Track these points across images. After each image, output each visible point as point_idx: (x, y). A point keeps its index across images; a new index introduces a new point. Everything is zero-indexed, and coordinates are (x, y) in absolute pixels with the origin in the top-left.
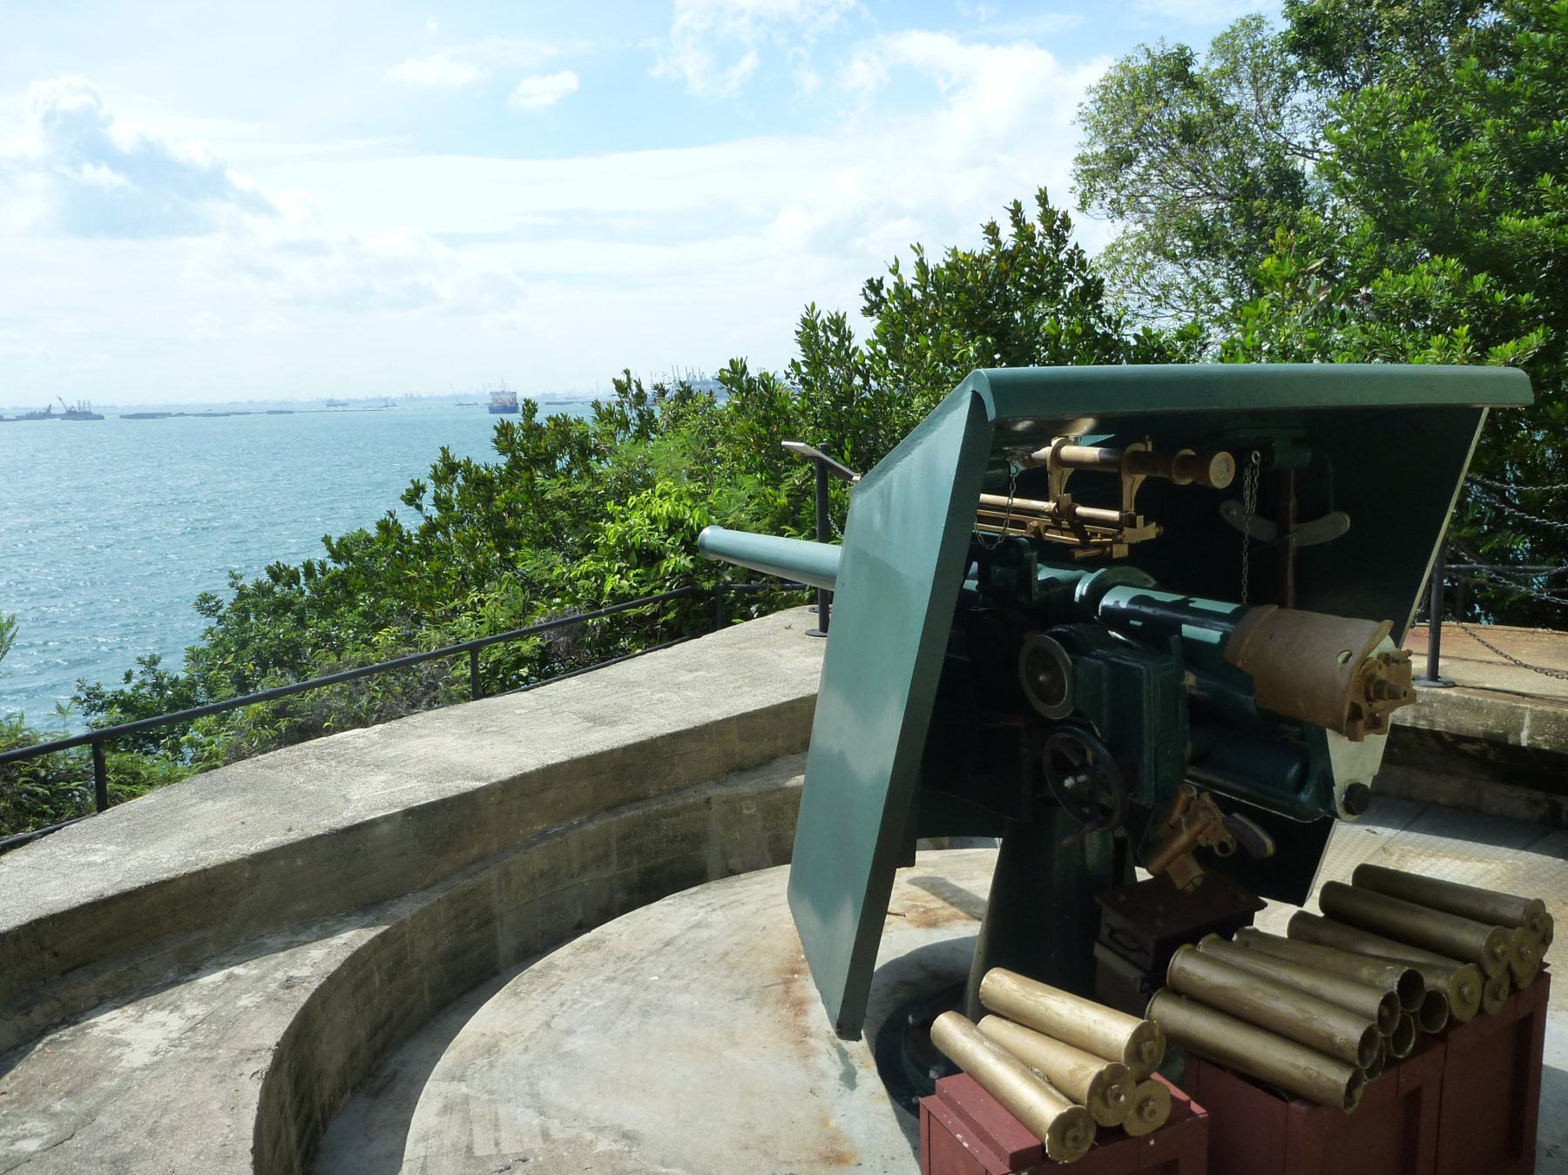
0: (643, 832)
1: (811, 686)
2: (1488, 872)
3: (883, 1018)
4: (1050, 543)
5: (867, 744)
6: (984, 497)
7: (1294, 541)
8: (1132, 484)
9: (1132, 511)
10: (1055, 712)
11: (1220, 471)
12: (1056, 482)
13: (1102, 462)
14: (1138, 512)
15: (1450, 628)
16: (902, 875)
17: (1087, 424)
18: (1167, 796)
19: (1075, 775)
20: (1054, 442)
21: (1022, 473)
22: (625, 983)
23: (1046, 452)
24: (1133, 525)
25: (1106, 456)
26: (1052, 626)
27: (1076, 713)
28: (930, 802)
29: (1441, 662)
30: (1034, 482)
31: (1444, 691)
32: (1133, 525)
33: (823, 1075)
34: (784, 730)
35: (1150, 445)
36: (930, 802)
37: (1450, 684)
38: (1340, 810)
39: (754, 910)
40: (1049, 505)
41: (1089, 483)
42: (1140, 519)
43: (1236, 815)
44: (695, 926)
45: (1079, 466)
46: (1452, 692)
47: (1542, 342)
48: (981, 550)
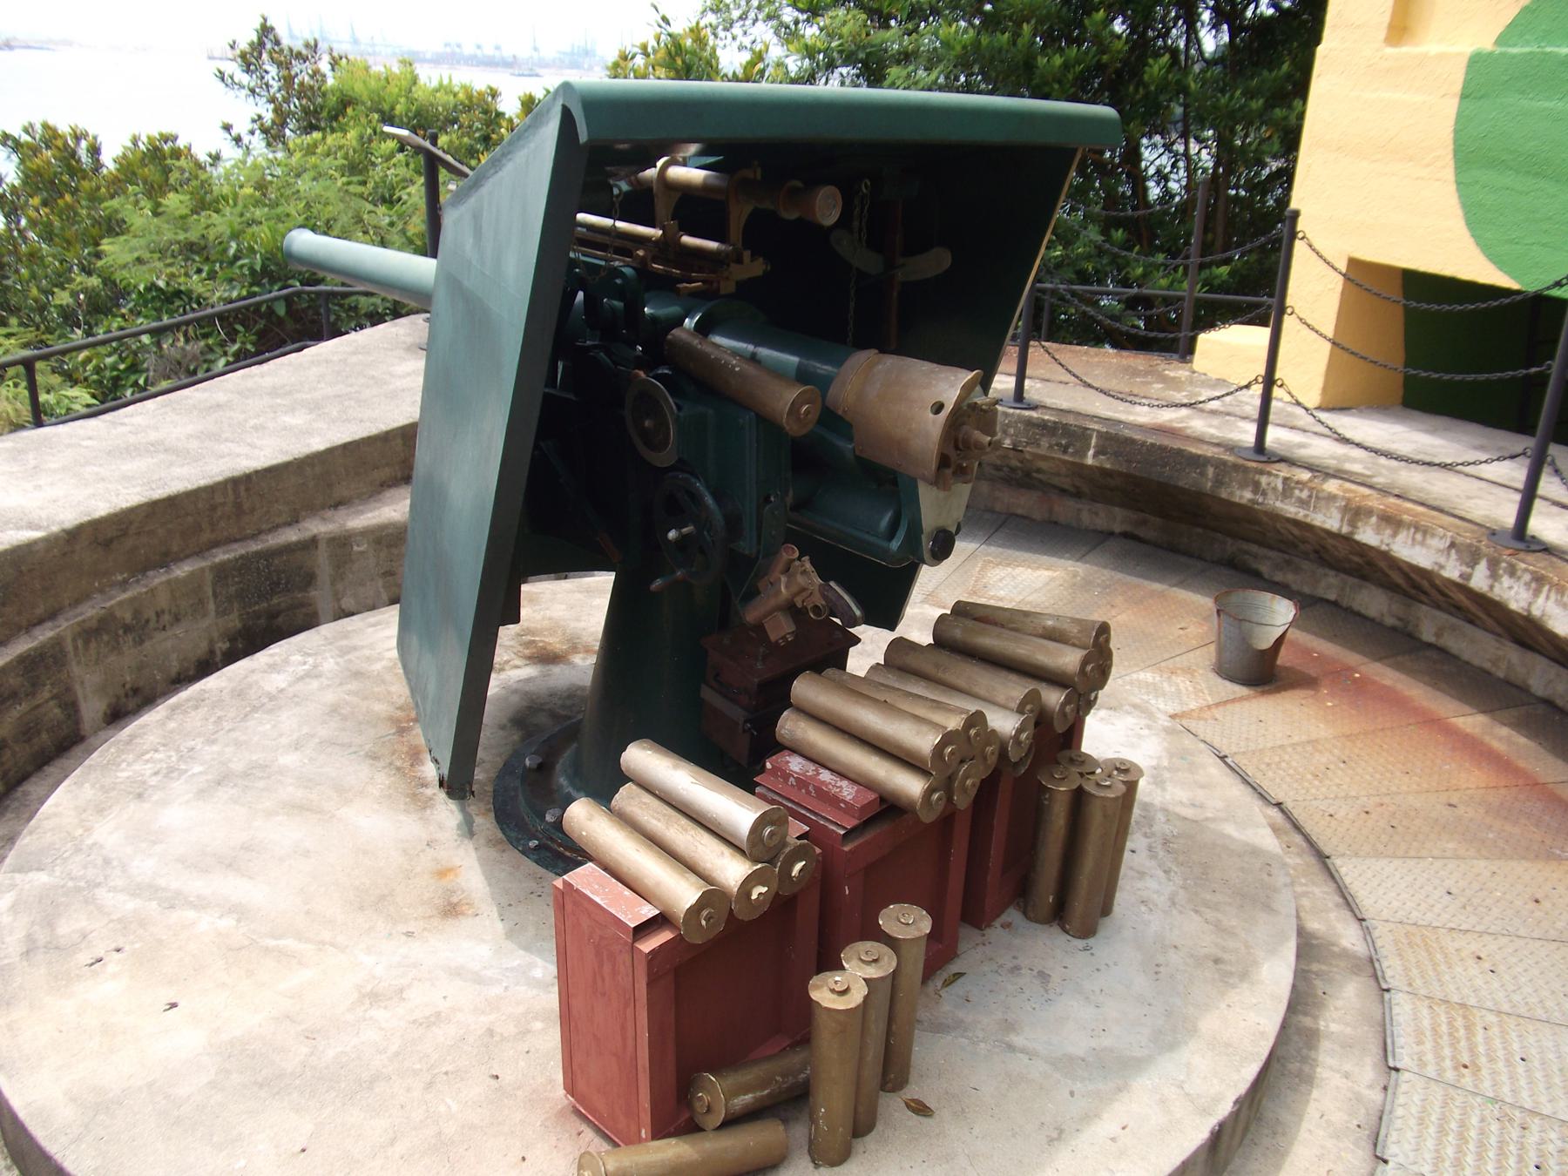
0: (233, 577)
1: (405, 411)
2: (1052, 579)
3: (500, 762)
4: (655, 273)
5: (471, 471)
6: (581, 217)
7: (900, 276)
8: (739, 214)
9: (740, 245)
10: (664, 458)
11: (827, 208)
12: (662, 208)
13: (705, 187)
14: (746, 245)
15: (1036, 351)
16: (506, 633)
17: (693, 148)
18: (771, 553)
19: (678, 527)
20: (660, 163)
21: (627, 194)
22: (227, 745)
23: (651, 173)
24: (739, 261)
25: (716, 182)
26: (657, 367)
27: (680, 460)
28: (538, 533)
29: (1027, 382)
30: (639, 205)
31: (1027, 413)
32: (739, 261)
33: (441, 827)
34: (385, 459)
35: (759, 172)
36: (538, 533)
37: (1035, 408)
38: (927, 556)
39: (355, 660)
40: (654, 232)
41: (692, 208)
42: (747, 254)
43: (832, 584)
44: (301, 678)
45: (685, 192)
46: (1034, 414)
47: (1244, 501)
48: (576, 278)
